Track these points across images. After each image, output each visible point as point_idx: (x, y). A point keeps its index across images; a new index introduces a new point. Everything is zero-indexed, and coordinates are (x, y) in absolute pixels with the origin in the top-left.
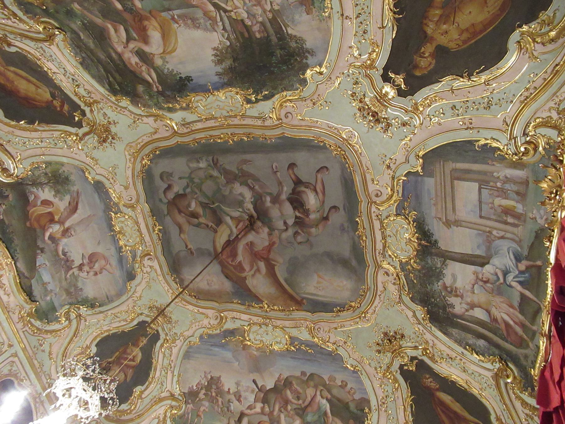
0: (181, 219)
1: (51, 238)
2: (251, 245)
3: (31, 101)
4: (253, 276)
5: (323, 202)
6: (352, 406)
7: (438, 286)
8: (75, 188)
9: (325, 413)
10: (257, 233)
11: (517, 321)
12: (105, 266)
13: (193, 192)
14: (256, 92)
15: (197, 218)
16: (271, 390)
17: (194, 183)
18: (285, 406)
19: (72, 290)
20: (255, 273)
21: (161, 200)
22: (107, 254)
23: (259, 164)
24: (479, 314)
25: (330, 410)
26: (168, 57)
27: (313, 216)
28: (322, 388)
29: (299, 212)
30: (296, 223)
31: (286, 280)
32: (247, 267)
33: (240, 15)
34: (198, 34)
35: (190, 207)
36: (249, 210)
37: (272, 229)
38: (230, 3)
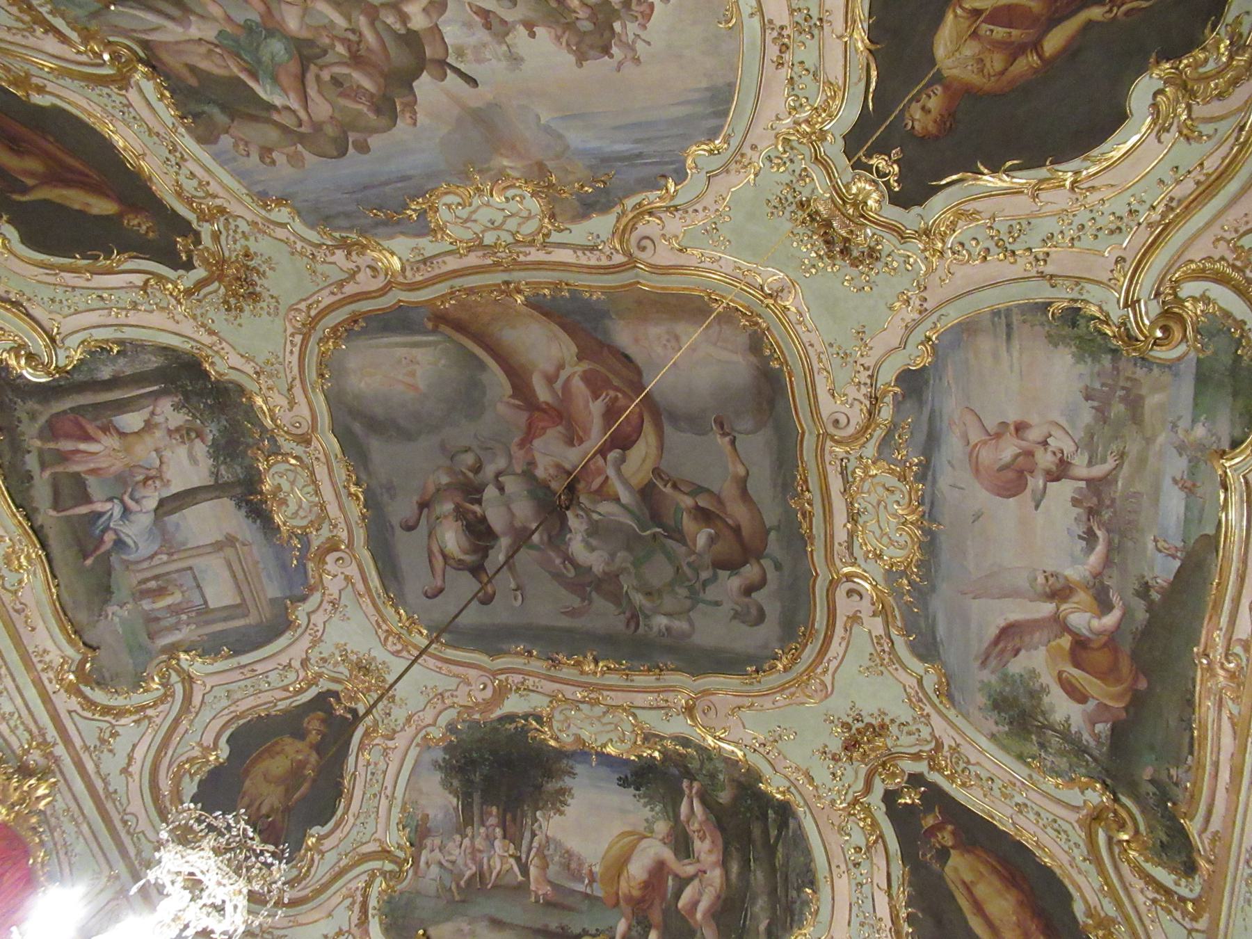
0: (738, 512)
1: (1104, 606)
2: (572, 439)
3: (1006, 874)
4: (561, 367)
5: (430, 536)
6: (221, 118)
7: (212, 431)
8: (986, 675)
9: (254, 75)
10: (558, 467)
11: (78, 457)
12: (985, 443)
13: (696, 569)
14: (524, 731)
15: (697, 507)
16: (417, 75)
17: (691, 588)
18: (354, 48)
19: (1118, 409)
20: (557, 376)
21: (778, 567)
22: (965, 476)
23: (549, 605)
24: (132, 421)
25: (252, 89)
26: (641, 829)
27: (448, 507)
28: (303, 129)
29: (474, 513)
30: (480, 489)
31: (482, 366)
32: (578, 385)
33: (504, 846)
34: (573, 843)
35: (710, 535)
36: (577, 516)
37: (528, 475)
38: (506, 867)
